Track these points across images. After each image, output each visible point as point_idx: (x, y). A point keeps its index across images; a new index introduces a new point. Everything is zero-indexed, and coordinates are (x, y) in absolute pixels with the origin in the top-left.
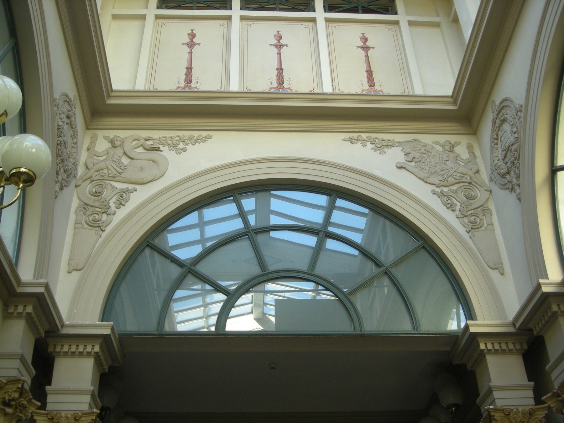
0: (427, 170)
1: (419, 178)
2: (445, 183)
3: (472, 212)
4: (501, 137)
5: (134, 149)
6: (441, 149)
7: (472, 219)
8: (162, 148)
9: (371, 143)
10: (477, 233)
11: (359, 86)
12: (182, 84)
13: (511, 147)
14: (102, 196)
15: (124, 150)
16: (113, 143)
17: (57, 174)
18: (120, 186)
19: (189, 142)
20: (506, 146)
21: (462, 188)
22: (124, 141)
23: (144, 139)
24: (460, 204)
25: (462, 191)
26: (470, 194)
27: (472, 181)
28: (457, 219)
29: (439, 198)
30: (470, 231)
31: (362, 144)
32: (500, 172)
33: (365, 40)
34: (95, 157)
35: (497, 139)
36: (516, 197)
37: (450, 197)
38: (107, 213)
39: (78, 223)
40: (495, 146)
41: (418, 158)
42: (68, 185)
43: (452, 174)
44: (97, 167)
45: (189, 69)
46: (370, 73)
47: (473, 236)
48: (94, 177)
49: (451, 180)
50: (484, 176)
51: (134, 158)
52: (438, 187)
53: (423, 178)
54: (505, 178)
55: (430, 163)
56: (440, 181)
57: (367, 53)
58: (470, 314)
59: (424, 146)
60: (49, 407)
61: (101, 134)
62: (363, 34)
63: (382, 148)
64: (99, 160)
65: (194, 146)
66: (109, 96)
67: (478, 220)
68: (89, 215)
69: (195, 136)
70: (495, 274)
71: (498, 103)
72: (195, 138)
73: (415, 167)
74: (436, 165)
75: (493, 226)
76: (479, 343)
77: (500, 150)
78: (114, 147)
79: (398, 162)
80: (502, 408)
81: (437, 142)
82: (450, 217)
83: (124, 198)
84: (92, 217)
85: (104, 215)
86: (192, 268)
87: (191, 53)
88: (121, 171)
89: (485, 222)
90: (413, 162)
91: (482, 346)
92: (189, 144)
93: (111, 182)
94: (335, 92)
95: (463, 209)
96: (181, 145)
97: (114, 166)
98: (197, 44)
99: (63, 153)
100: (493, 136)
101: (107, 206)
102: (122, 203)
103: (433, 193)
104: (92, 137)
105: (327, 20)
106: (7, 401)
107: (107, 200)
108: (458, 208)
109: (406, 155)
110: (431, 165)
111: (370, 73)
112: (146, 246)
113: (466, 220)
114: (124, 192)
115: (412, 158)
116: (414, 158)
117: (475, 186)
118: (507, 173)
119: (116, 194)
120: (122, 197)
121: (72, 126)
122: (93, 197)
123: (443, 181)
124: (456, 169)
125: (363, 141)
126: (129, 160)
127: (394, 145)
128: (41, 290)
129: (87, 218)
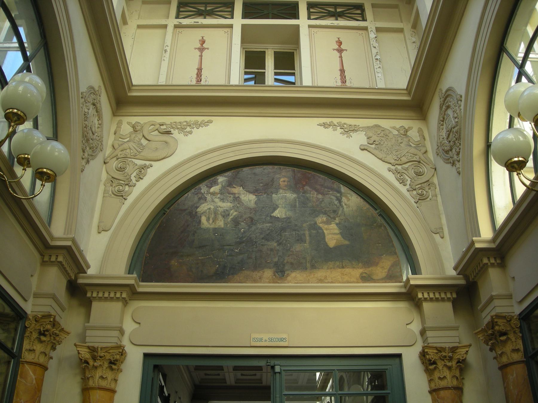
0: (385, 151)
1: (378, 158)
2: (399, 162)
3: (420, 186)
4: (446, 120)
5: (151, 133)
6: (396, 133)
7: (420, 191)
9: (340, 128)
10: (423, 203)
12: (194, 82)
13: (453, 129)
14: (126, 171)
15: (143, 134)
16: (135, 128)
17: (84, 152)
18: (139, 162)
19: (194, 126)
20: (449, 128)
21: (412, 166)
22: (143, 127)
23: (159, 124)
24: (410, 179)
25: (413, 168)
26: (419, 171)
27: (421, 160)
28: (408, 192)
29: (394, 175)
30: (418, 202)
31: (333, 129)
32: (444, 148)
33: (340, 43)
34: (120, 139)
35: (443, 121)
36: (456, 171)
37: (403, 173)
38: (129, 185)
39: (107, 193)
40: (441, 126)
41: (378, 141)
42: (94, 158)
43: (405, 155)
44: (121, 148)
45: (200, 70)
46: (342, 71)
47: (420, 206)
48: (119, 155)
49: (404, 159)
50: (431, 155)
51: (150, 140)
52: (393, 165)
53: (382, 158)
54: (447, 154)
55: (387, 145)
56: (395, 160)
57: (341, 55)
58: (415, 270)
59: (383, 131)
61: (126, 120)
62: (339, 38)
63: (349, 132)
64: (124, 142)
65: (198, 129)
66: (130, 89)
67: (425, 193)
68: (115, 187)
69: (199, 122)
70: (437, 237)
71: (444, 91)
72: (199, 123)
73: (375, 149)
74: (392, 146)
75: (437, 197)
76: (418, 293)
77: (445, 130)
78: (136, 131)
79: (361, 145)
80: (504, 314)
81: (394, 127)
83: (142, 173)
84: (117, 188)
85: (127, 187)
87: (201, 56)
88: (141, 151)
89: (430, 194)
90: (373, 144)
91: (420, 295)
92: (194, 128)
93: (132, 159)
94: (314, 85)
95: (413, 183)
96: (188, 129)
98: (206, 48)
99: (88, 134)
100: (440, 118)
101: (129, 180)
102: (141, 177)
103: (389, 170)
104: (118, 123)
105: (310, 26)
106: (42, 332)
107: (129, 174)
108: (408, 182)
109: (368, 138)
110: (388, 147)
111: (342, 71)
113: (415, 192)
114: (143, 168)
115: (373, 141)
116: (375, 141)
117: (423, 164)
118: (450, 150)
119: (137, 169)
120: (141, 172)
121: (98, 111)
122: (118, 172)
123: (398, 161)
124: (408, 150)
125: (334, 126)
126: (148, 142)
127: (359, 130)
128: (69, 243)
129: (113, 189)
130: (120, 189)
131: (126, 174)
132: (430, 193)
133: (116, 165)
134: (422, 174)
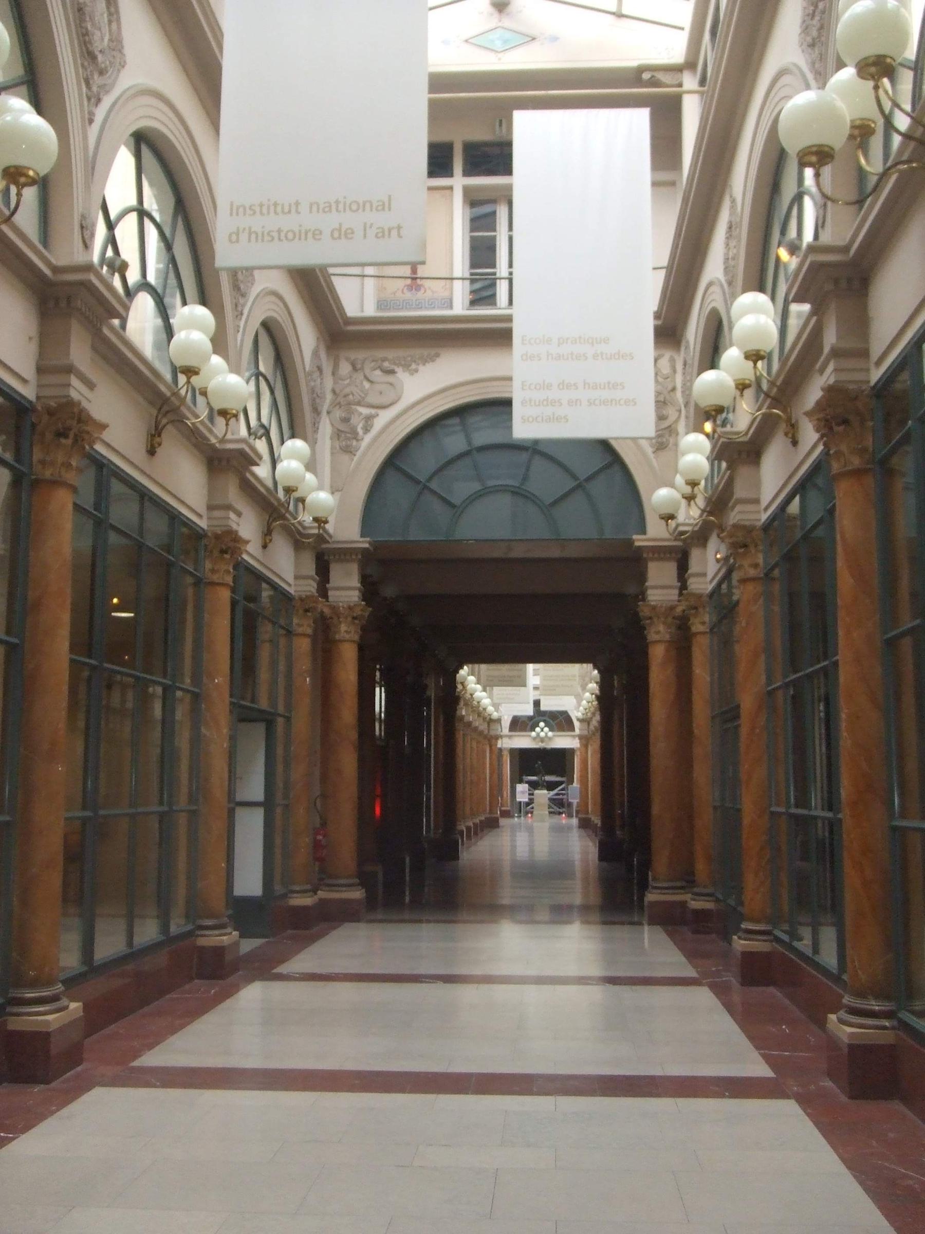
8: (397, 369)
11: (403, 290)
18: (362, 410)
34: (340, 382)
60: (330, 599)
84: (344, 443)
86: (428, 484)
97: (358, 391)
112: (233, 738)
132: (672, 440)
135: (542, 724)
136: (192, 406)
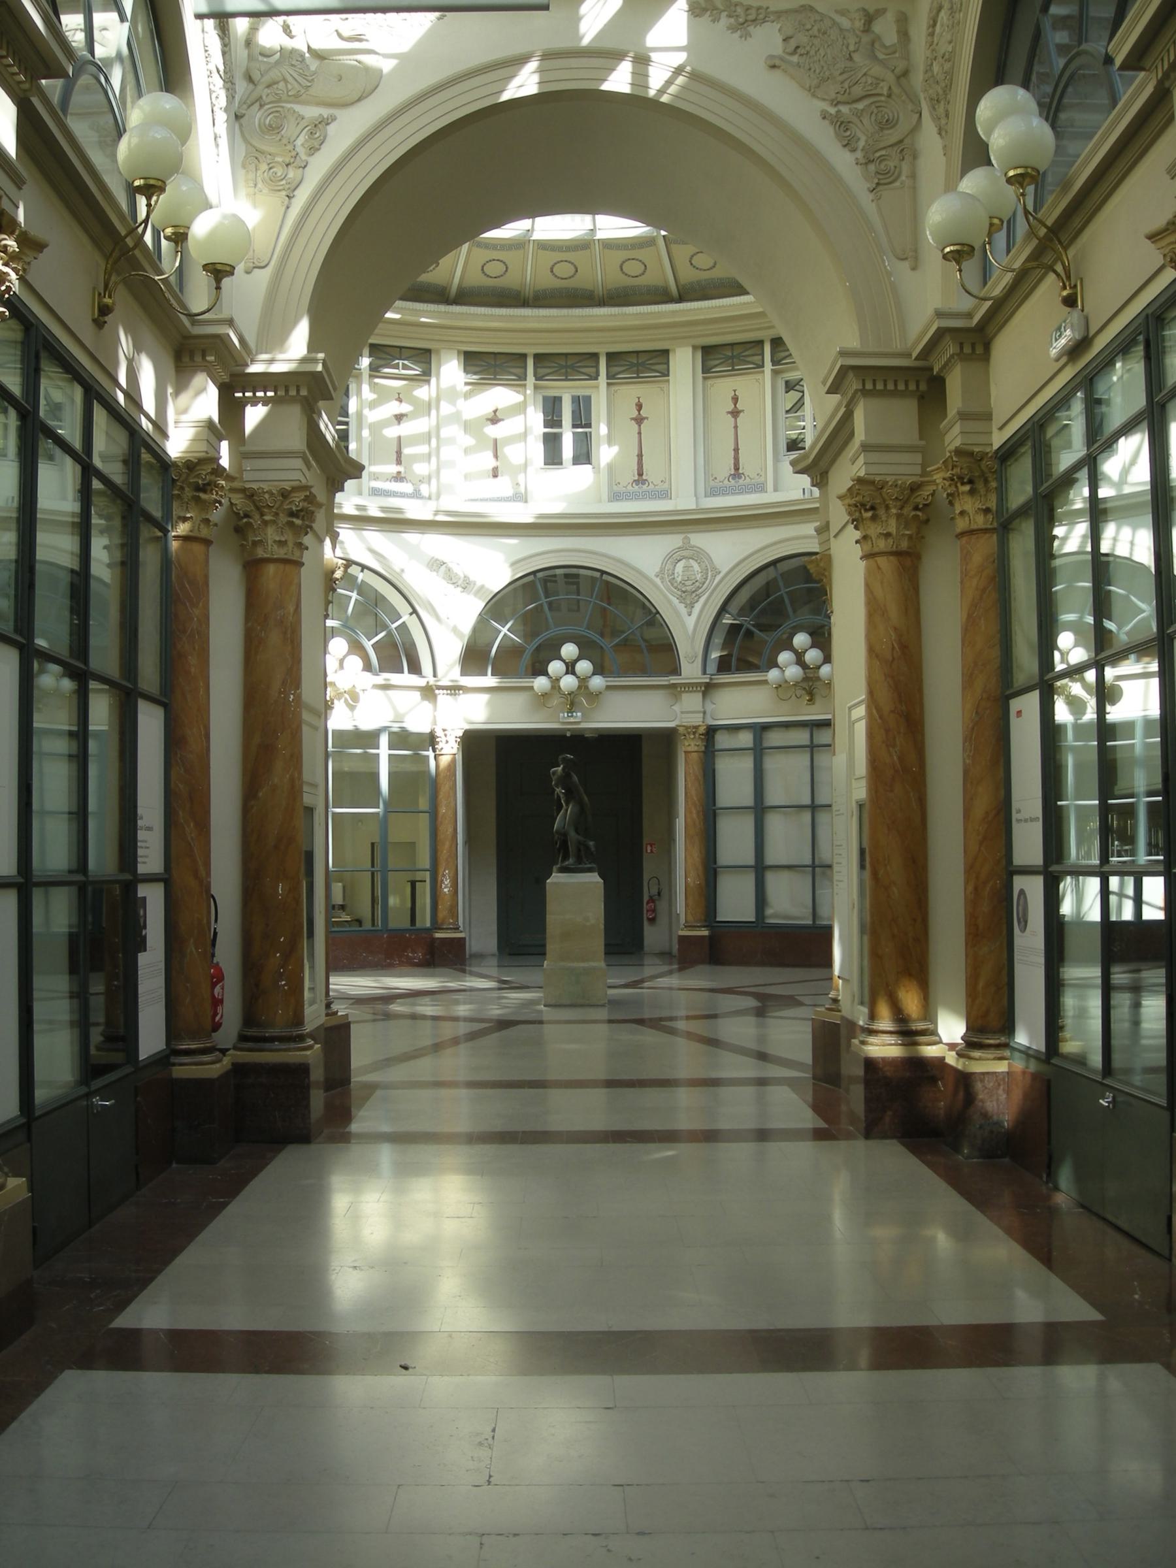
18: (311, 112)
44: (267, 79)
48: (264, 97)
49: (858, 91)
82: (844, 162)
88: (309, 84)
130: (279, 174)
131: (285, 141)
133: (260, 119)
134: (894, 122)
135: (569, 650)
136: (178, 290)
